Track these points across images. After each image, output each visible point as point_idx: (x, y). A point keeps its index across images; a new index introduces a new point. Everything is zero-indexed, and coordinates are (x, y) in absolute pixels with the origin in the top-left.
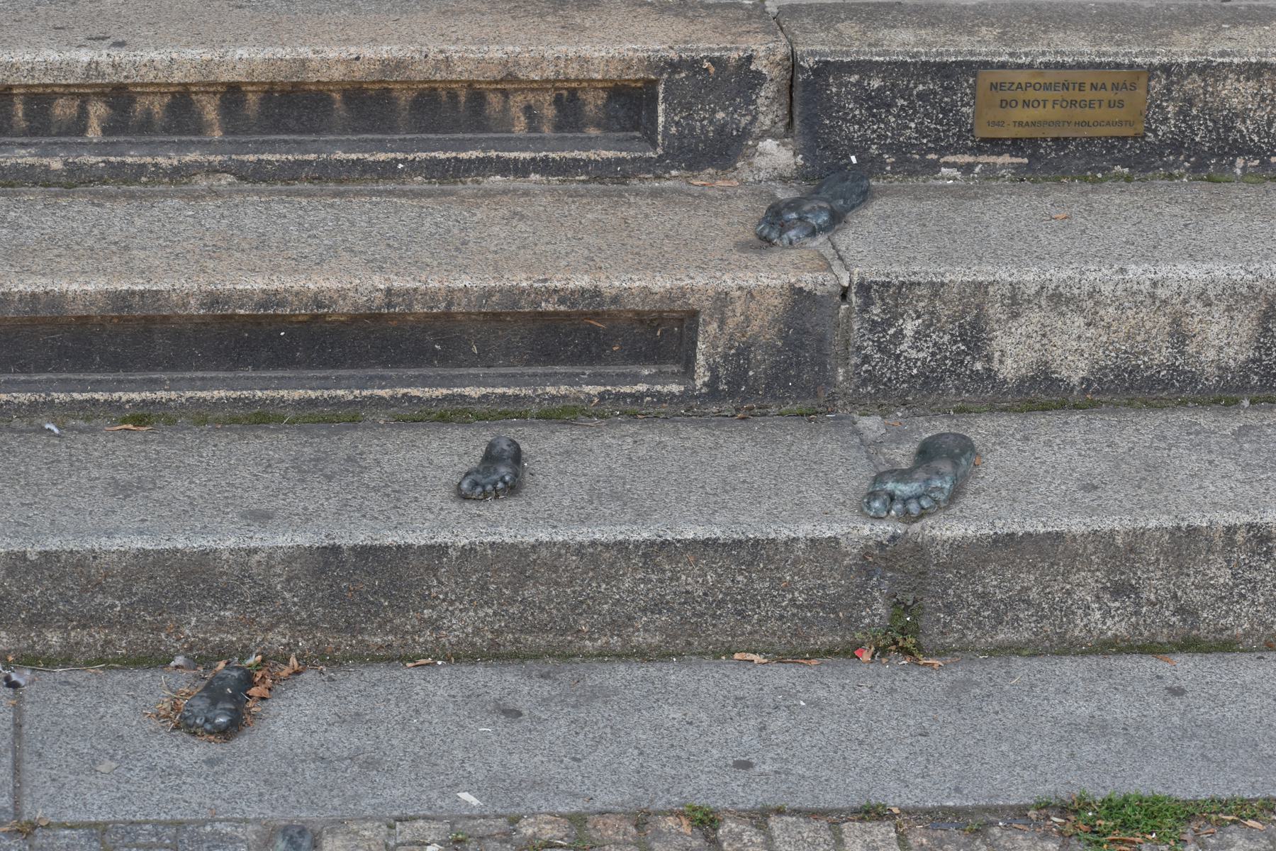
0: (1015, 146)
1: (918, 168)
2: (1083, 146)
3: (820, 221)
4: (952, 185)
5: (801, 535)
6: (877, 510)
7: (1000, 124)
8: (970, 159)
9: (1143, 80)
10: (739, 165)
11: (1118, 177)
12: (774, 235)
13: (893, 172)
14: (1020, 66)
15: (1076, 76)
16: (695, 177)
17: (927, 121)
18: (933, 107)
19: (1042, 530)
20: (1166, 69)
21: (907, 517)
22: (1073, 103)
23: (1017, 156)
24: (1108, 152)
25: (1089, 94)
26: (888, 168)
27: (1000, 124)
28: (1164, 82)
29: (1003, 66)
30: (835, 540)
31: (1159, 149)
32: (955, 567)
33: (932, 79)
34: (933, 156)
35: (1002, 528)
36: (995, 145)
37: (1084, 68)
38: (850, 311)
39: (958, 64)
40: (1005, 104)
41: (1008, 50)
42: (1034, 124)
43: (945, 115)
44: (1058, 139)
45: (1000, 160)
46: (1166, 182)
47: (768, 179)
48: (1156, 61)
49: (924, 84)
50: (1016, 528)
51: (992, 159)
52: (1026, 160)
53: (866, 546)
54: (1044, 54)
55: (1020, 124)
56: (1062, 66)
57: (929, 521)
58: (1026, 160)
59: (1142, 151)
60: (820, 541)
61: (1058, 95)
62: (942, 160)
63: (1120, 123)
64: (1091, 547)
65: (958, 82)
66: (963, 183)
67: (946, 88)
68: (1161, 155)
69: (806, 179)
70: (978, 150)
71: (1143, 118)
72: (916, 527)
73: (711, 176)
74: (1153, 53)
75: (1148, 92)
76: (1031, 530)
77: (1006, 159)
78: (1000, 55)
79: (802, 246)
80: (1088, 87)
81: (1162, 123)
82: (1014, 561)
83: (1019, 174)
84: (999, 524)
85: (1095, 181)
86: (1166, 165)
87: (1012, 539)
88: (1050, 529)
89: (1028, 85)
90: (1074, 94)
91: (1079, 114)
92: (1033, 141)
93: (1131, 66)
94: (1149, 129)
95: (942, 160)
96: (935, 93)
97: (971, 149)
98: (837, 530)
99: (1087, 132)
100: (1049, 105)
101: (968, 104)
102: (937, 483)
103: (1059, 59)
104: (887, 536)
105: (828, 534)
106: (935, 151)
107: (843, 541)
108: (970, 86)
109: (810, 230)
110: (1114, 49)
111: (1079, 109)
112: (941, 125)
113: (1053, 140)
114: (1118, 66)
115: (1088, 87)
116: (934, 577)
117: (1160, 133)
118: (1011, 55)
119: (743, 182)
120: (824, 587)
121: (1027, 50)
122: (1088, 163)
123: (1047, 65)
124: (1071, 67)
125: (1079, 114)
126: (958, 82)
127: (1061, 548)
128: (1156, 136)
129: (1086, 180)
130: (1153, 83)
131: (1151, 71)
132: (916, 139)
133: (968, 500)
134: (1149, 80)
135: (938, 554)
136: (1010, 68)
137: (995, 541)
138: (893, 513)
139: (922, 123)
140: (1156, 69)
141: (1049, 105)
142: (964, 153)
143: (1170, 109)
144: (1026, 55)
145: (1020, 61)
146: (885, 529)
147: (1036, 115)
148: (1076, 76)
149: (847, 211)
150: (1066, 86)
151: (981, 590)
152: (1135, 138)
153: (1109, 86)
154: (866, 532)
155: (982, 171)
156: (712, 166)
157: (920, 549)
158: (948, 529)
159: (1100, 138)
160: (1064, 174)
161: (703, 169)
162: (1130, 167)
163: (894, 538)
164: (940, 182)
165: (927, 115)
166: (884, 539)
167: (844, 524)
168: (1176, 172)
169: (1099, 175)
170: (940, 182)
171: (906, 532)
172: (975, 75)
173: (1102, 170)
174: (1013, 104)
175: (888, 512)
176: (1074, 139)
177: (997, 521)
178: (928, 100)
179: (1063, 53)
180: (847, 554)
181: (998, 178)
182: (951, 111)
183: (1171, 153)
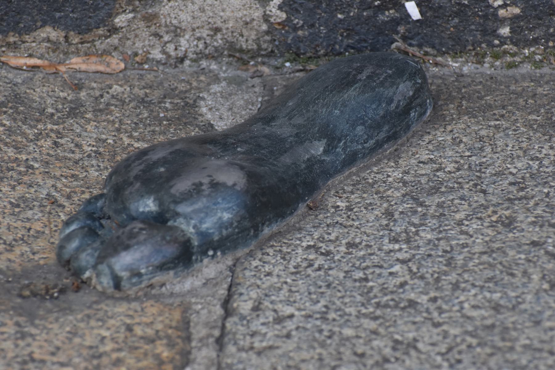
3: (208, 225)
10: (120, 20)
12: (86, 258)
13: (518, 39)
16: (14, 47)
26: (505, 31)
38: (545, 358)
47: (201, 56)
69: (296, 56)
73: (55, 46)
79: (149, 293)
109: (171, 251)
119: (136, 62)
149: (328, 173)
156: (55, 23)
161: (29, 30)
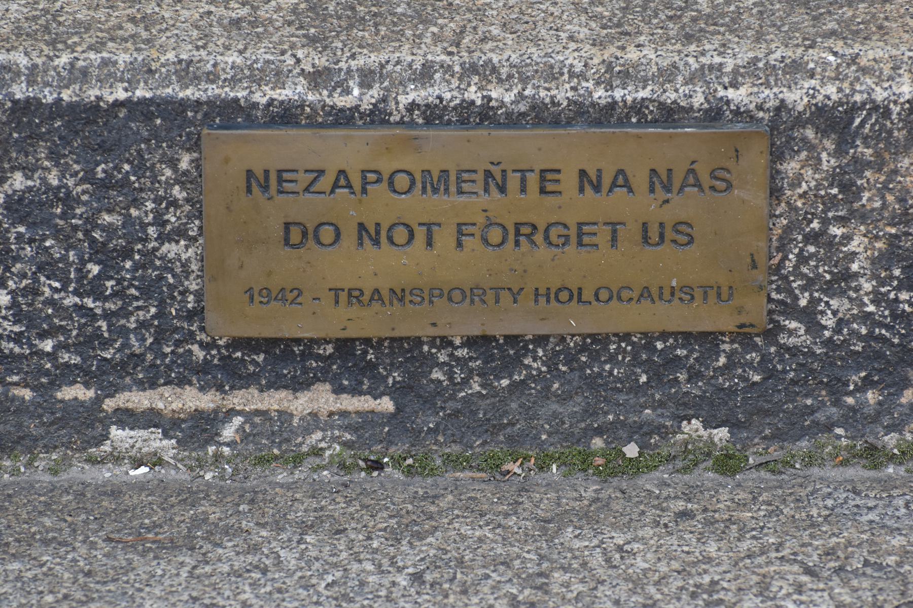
0: (349, 361)
1: (33, 427)
2: (571, 360)
4: (141, 486)
7: (290, 295)
8: (207, 401)
9: (756, 158)
11: (692, 457)
14: (343, 118)
15: (533, 147)
17: (48, 286)
18: (66, 239)
20: (835, 121)
22: (523, 232)
23: (356, 391)
24: (656, 377)
25: (574, 205)
27: (290, 295)
28: (828, 162)
29: (286, 115)
31: (828, 369)
33: (55, 156)
34: (77, 392)
36: (285, 360)
37: (556, 122)
39: (141, 110)
40: (297, 235)
41: (312, 59)
42: (399, 295)
43: (110, 266)
44: (487, 339)
45: (301, 404)
46: (855, 472)
48: (797, 97)
49: (28, 171)
51: (274, 401)
52: (386, 404)
54: (425, 75)
55: (355, 296)
56: (486, 115)
58: (386, 404)
59: (771, 374)
61: (476, 204)
62: (109, 404)
63: (687, 292)
65: (140, 168)
66: (183, 475)
67: (105, 185)
68: (837, 387)
70: (226, 371)
71: (760, 276)
74: (795, 68)
75: (775, 193)
77: (321, 399)
78: (280, 78)
80: (569, 180)
81: (830, 289)
83: (367, 448)
85: (616, 468)
86: (853, 418)
89: (370, 178)
90: (531, 206)
91: (543, 263)
92: (408, 350)
93: (714, 113)
94: (790, 309)
95: (109, 404)
96: (69, 201)
97: (204, 369)
99: (575, 322)
100: (445, 238)
101: (180, 233)
103: (473, 94)
106: (88, 377)
108: (182, 179)
110: (668, 56)
111: (543, 252)
112: (99, 296)
113: (470, 342)
114: (670, 115)
115: (569, 180)
117: (828, 321)
118: (317, 78)
121: (371, 59)
122: (590, 412)
123: (434, 114)
124: (513, 120)
125: (543, 263)
126: (140, 168)
128: (814, 327)
129: (585, 461)
130: (791, 167)
131: (780, 131)
132: (17, 338)
134: (777, 156)
136: (313, 124)
139: (33, 291)
140: (799, 121)
141: (445, 238)
142: (182, 382)
143: (855, 245)
144: (367, 78)
145: (341, 101)
147: (427, 269)
148: (533, 147)
150: (494, 181)
152: (743, 336)
153: (640, 180)
155: (246, 437)
159: (626, 337)
160: (515, 447)
162: (734, 425)
164: (106, 473)
165: (48, 267)
168: (891, 440)
169: (631, 450)
170: (106, 473)
172: (195, 145)
173: (640, 432)
174: (327, 234)
176: (542, 340)
178: (47, 222)
179: (486, 72)
181: (298, 460)
182: (127, 253)
183: (867, 383)
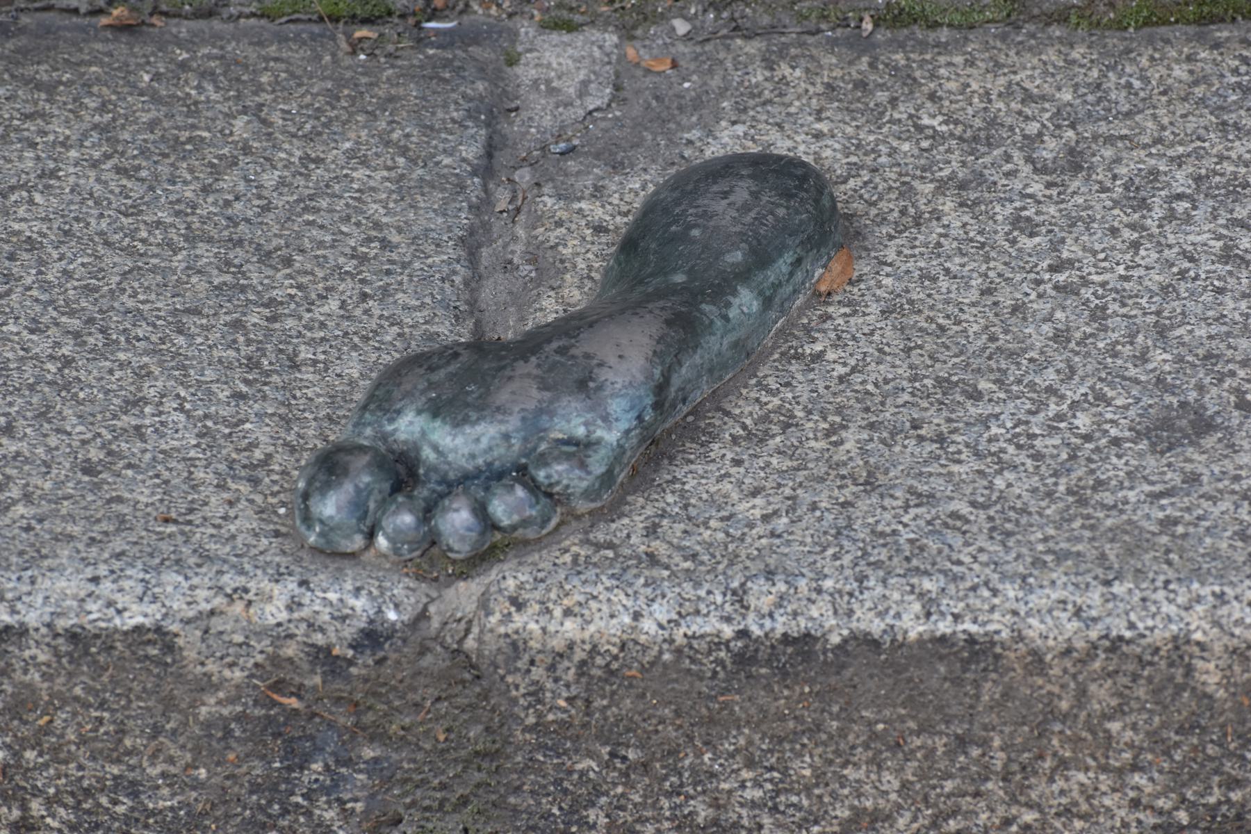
5: (32, 619)
6: (329, 529)
19: (913, 627)
21: (429, 559)
30: (160, 635)
32: (603, 738)
35: (768, 613)
50: (822, 618)
53: (275, 660)
57: (511, 577)
60: (106, 639)
64: (1101, 695)
72: (463, 596)
76: (876, 627)
82: (819, 727)
84: (762, 596)
87: (808, 656)
88: (945, 627)
98: (178, 597)
102: (572, 421)
104: (349, 632)
105: (137, 616)
107: (189, 641)
116: (531, 765)
120: (134, 790)
127: (989, 690)
133: (710, 477)
135: (536, 693)
137: (744, 660)
138: (382, 542)
146: (346, 602)
151: (704, 813)
154: (274, 612)
157: (469, 675)
158: (572, 611)
163: (372, 637)
166: (339, 638)
167: (204, 578)
171: (423, 616)
175: (371, 536)
177: (757, 586)
180: (206, 685)
